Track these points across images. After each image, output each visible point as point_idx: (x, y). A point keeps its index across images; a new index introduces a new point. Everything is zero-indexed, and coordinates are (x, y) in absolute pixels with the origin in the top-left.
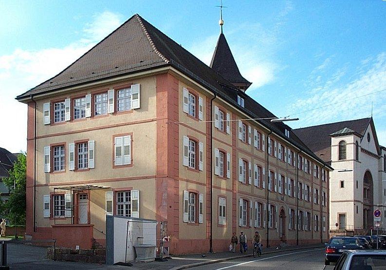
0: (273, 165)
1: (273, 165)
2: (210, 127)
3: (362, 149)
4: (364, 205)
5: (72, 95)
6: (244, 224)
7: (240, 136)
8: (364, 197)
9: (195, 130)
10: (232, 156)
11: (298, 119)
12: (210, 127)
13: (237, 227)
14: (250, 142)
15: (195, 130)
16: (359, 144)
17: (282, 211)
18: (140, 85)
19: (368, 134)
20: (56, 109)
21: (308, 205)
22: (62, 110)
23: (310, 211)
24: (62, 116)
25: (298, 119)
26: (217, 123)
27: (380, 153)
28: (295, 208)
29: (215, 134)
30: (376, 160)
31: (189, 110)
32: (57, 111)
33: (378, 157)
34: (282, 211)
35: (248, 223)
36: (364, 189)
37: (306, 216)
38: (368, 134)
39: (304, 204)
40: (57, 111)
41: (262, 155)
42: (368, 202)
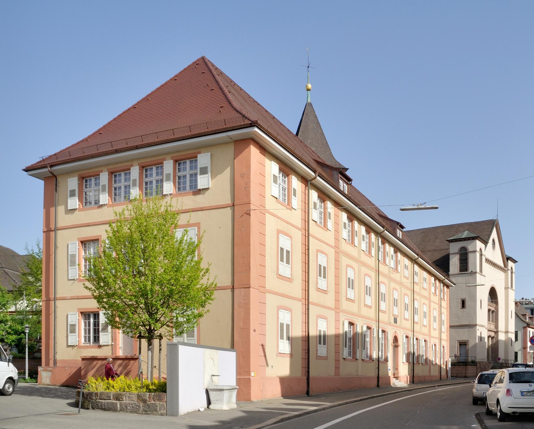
0: (385, 276)
1: (385, 276)
2: (307, 221)
3: (487, 261)
4: (250, 400)
5: (111, 167)
6: (350, 355)
7: (345, 234)
8: (489, 320)
9: (288, 223)
10: (253, 282)
11: (436, 208)
12: (307, 221)
13: (341, 360)
14: (356, 243)
15: (288, 223)
16: (483, 253)
17: (396, 339)
18: (211, 155)
19: (493, 240)
20: (146, 177)
21: (425, 330)
22: (127, 183)
23: (428, 339)
24: (125, 192)
25: (436, 208)
26: (315, 215)
27: (506, 265)
28: (410, 335)
29: (314, 229)
30: (501, 274)
31: (279, 193)
32: (117, 185)
33: (504, 269)
34: (396, 339)
35: (355, 353)
36: (489, 310)
37: (423, 345)
38: (493, 240)
39: (421, 328)
40: (117, 185)
41: (372, 262)
42: (493, 327)
